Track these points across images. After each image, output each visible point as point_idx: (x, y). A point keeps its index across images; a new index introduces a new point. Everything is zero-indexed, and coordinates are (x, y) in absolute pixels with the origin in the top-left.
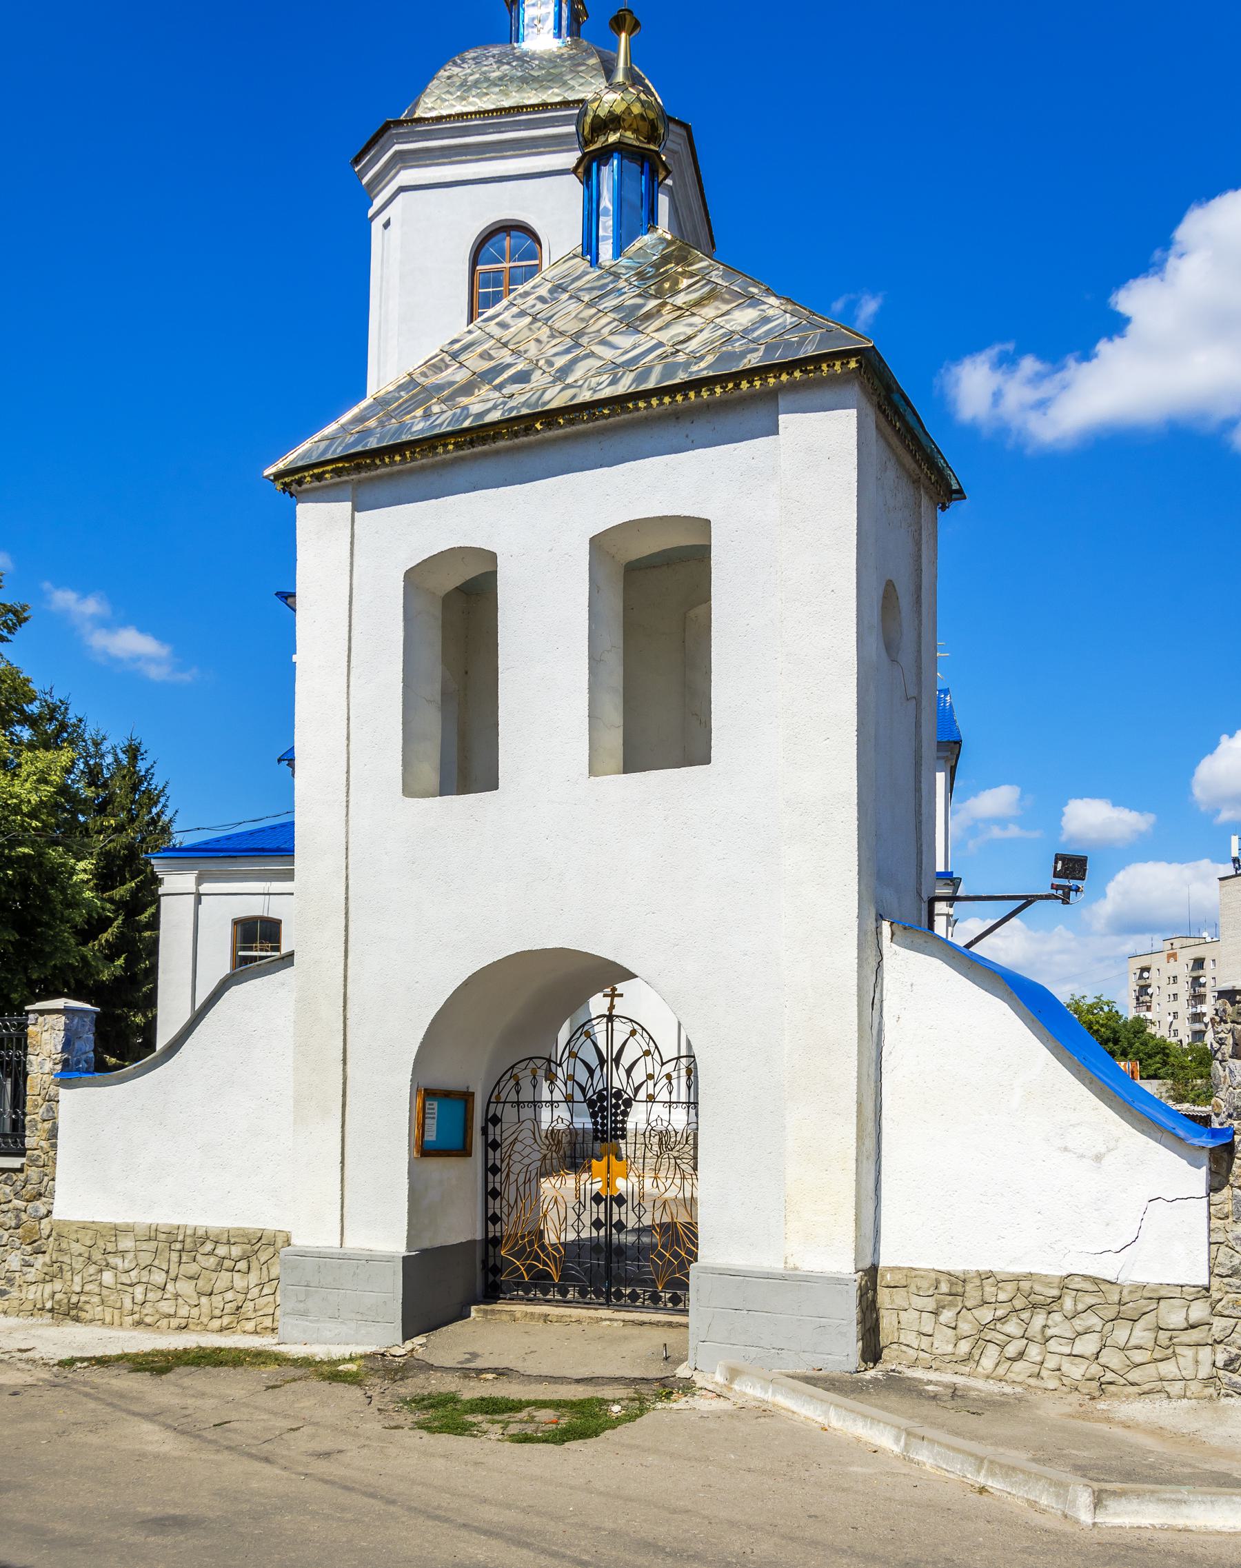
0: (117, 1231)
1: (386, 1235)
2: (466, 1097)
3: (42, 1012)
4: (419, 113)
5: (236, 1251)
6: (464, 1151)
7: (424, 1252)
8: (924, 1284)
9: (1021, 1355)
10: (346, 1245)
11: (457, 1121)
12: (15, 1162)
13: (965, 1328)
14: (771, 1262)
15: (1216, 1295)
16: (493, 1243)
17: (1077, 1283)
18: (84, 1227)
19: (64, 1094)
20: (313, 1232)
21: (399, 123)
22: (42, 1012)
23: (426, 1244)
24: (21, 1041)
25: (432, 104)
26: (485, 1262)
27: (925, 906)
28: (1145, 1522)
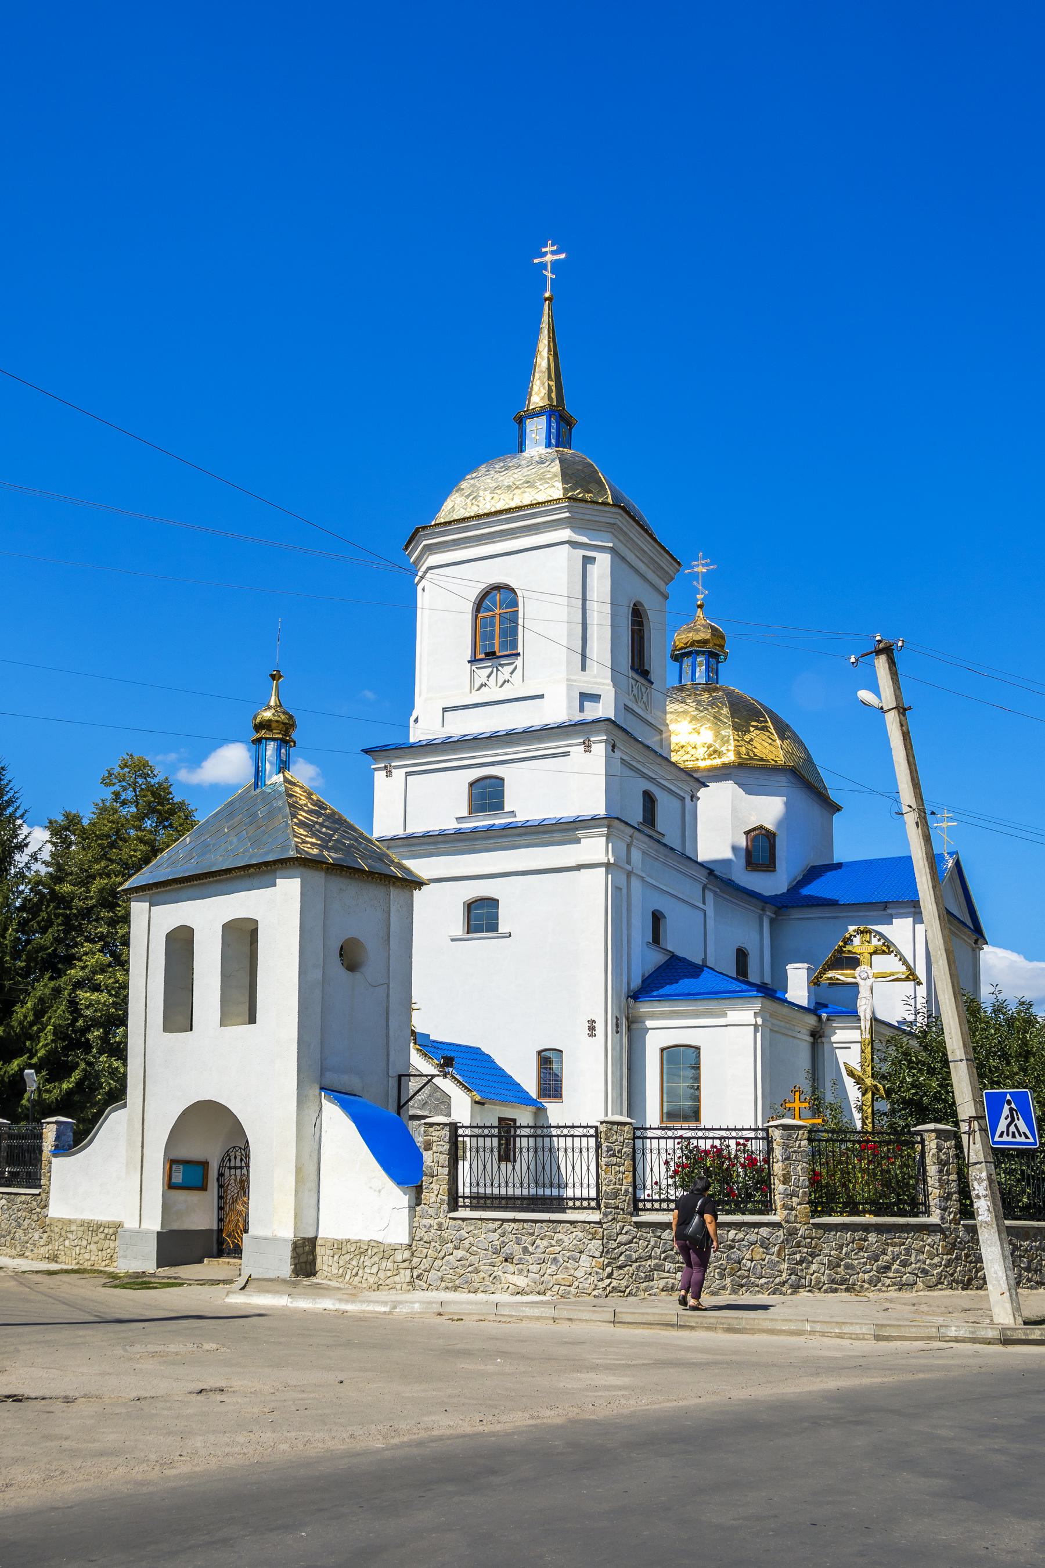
0: (71, 1222)
1: (154, 1224)
2: (204, 1165)
3: (48, 1123)
4: (442, 517)
5: (111, 1231)
6: (203, 1188)
7: (173, 1233)
8: (330, 1244)
9: (357, 1274)
10: (143, 1227)
11: (185, 1174)
12: (36, 1191)
13: (342, 1263)
14: (268, 1234)
15: (414, 1248)
16: (220, 1231)
17: (373, 1244)
18: (59, 1220)
19: (54, 1160)
20: (131, 1223)
21: (424, 528)
22: (48, 1123)
23: (175, 1226)
24: (40, 1136)
25: (456, 505)
26: (218, 1240)
27: (393, 1083)
28: (238, 1301)
